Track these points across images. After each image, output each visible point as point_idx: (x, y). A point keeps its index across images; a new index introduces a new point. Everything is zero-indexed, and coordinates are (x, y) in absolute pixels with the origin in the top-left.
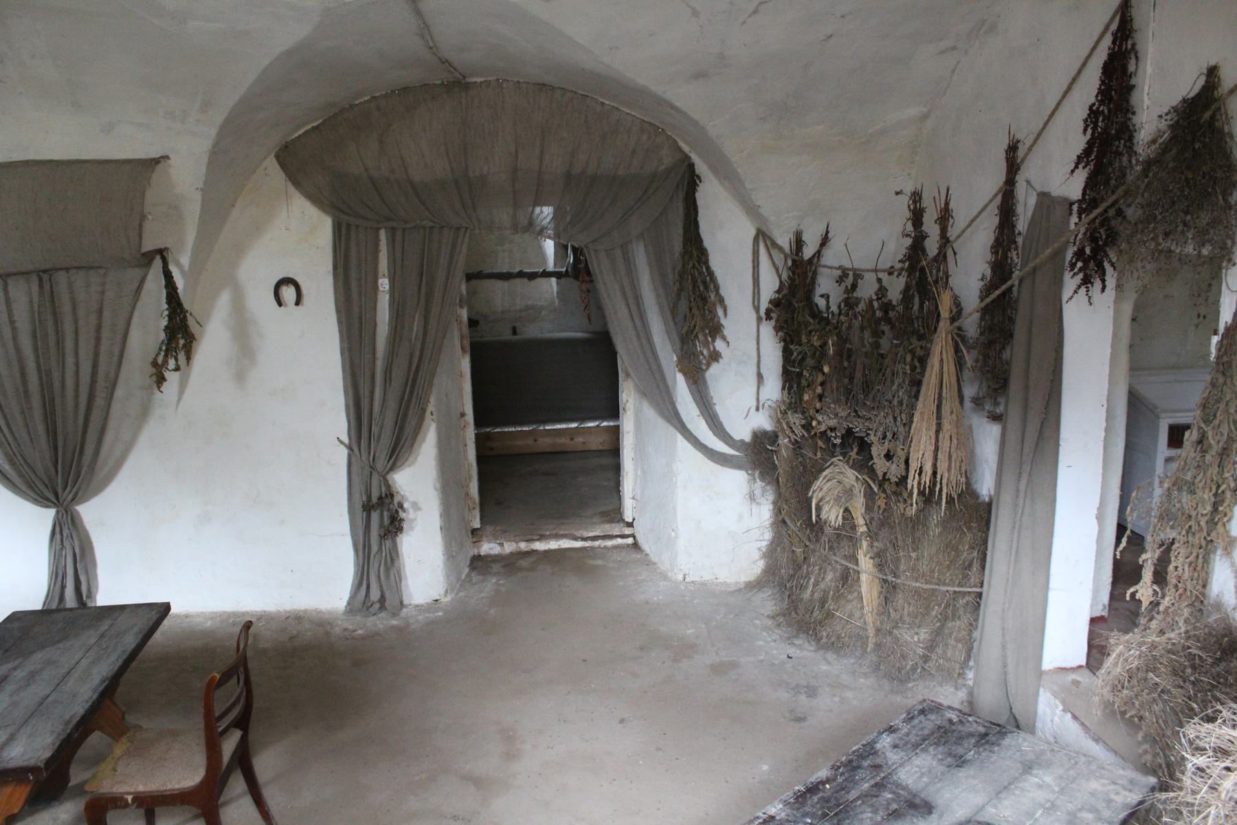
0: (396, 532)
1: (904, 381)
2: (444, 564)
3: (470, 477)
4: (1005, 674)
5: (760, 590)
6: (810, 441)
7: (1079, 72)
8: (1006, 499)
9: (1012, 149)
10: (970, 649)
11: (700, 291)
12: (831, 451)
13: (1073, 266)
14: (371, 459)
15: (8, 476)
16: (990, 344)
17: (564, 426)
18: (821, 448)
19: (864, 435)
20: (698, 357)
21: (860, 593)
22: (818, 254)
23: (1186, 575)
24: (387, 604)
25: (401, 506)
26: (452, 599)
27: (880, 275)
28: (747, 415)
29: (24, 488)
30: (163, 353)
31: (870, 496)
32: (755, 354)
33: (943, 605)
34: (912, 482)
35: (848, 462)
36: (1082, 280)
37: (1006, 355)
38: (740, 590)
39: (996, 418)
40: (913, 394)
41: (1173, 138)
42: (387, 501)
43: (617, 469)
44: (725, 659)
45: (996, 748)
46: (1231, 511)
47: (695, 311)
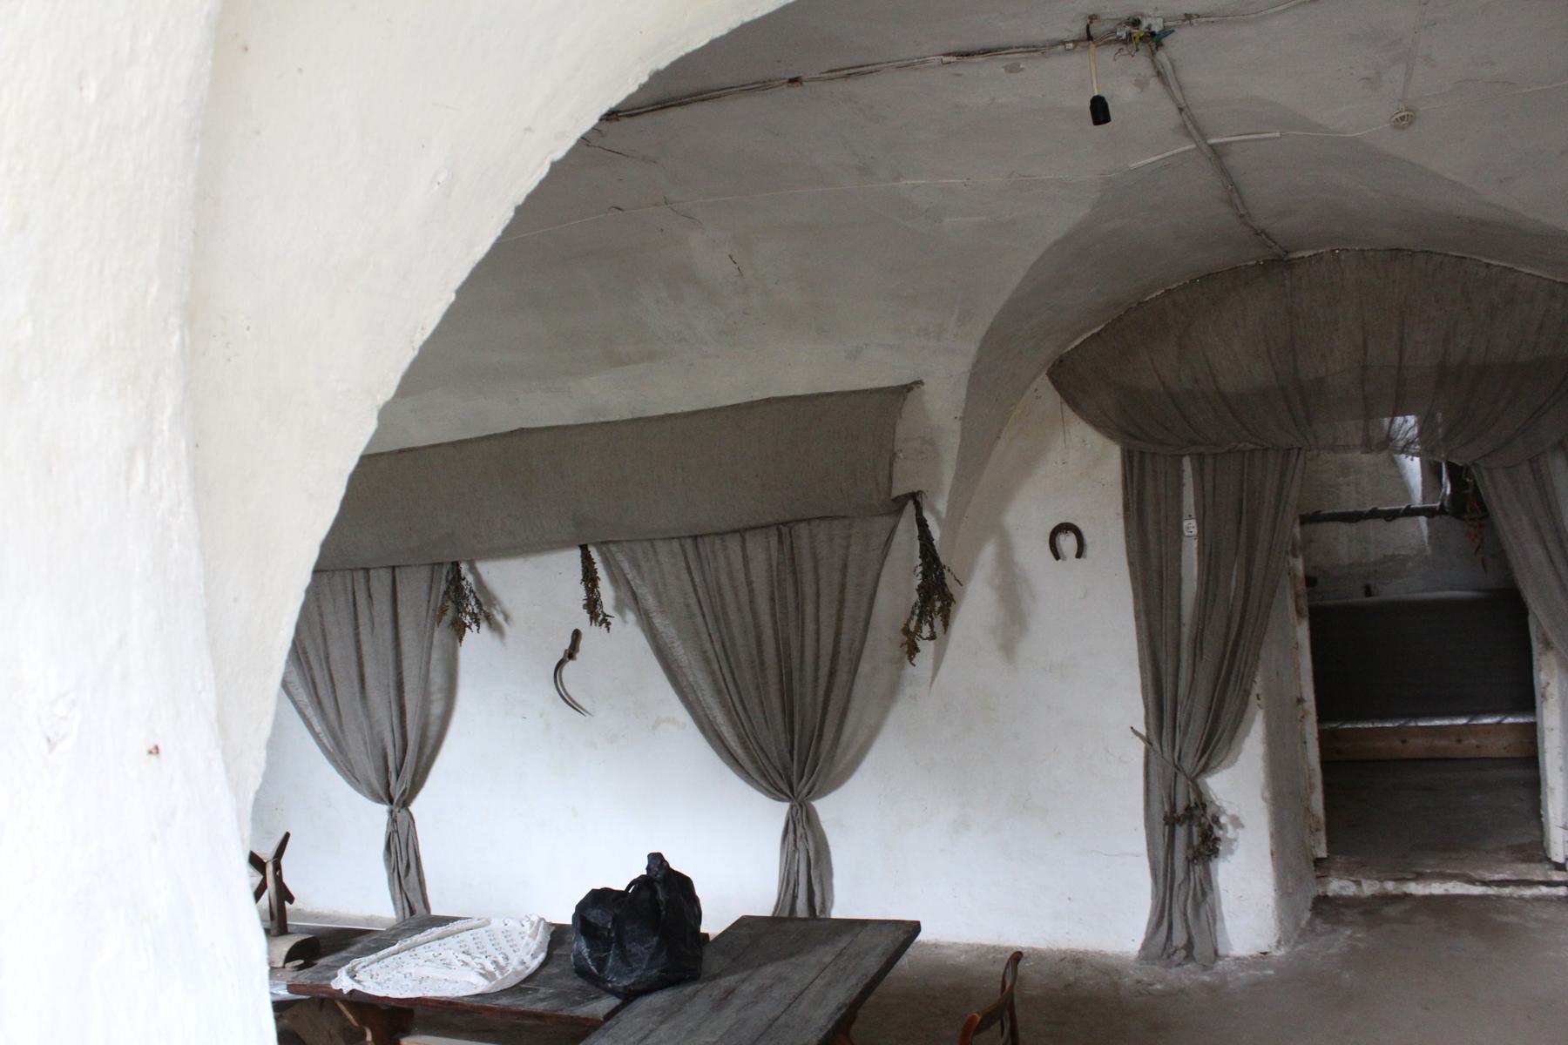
0: (1209, 856)
3: (1312, 786)
15: (740, 762)
17: (1446, 722)
24: (1196, 952)
25: (1216, 820)
26: (1288, 953)
29: (756, 776)
30: (916, 618)
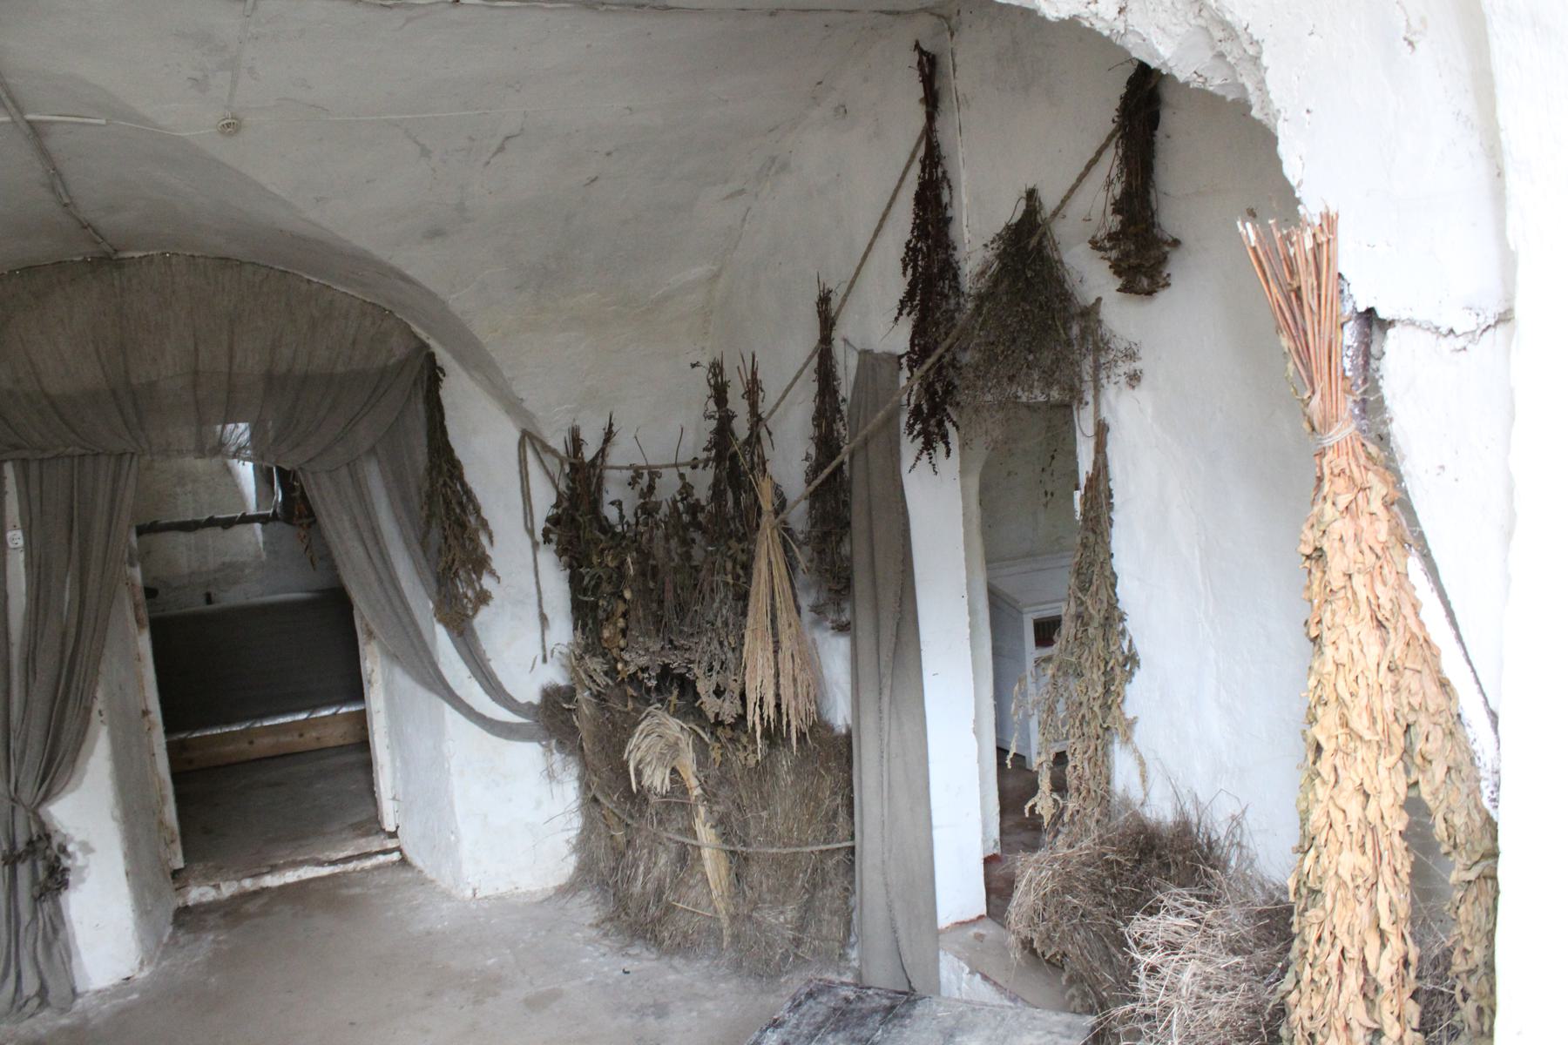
0: (58, 889)
1: (726, 596)
2: (136, 924)
3: (163, 798)
4: (897, 941)
5: (575, 894)
6: (617, 690)
7: (890, 206)
8: (868, 722)
9: (824, 300)
10: (849, 923)
11: (455, 513)
12: (645, 697)
13: (911, 427)
14: (12, 787)
16: (825, 537)
17: (288, 719)
18: (632, 696)
19: (683, 671)
20: (461, 601)
21: (704, 874)
22: (602, 453)
23: (1087, 773)
24: (51, 997)
25: (63, 849)
27: (682, 470)
28: (533, 668)
31: (701, 748)
32: (534, 590)
33: (809, 871)
34: (753, 717)
35: (668, 710)
36: (923, 443)
37: (845, 549)
38: (548, 899)
39: (842, 628)
40: (739, 611)
41: (1004, 267)
42: (41, 845)
43: (368, 766)
44: (543, 989)
45: (908, 1021)
46: (1123, 690)
47: (451, 541)
